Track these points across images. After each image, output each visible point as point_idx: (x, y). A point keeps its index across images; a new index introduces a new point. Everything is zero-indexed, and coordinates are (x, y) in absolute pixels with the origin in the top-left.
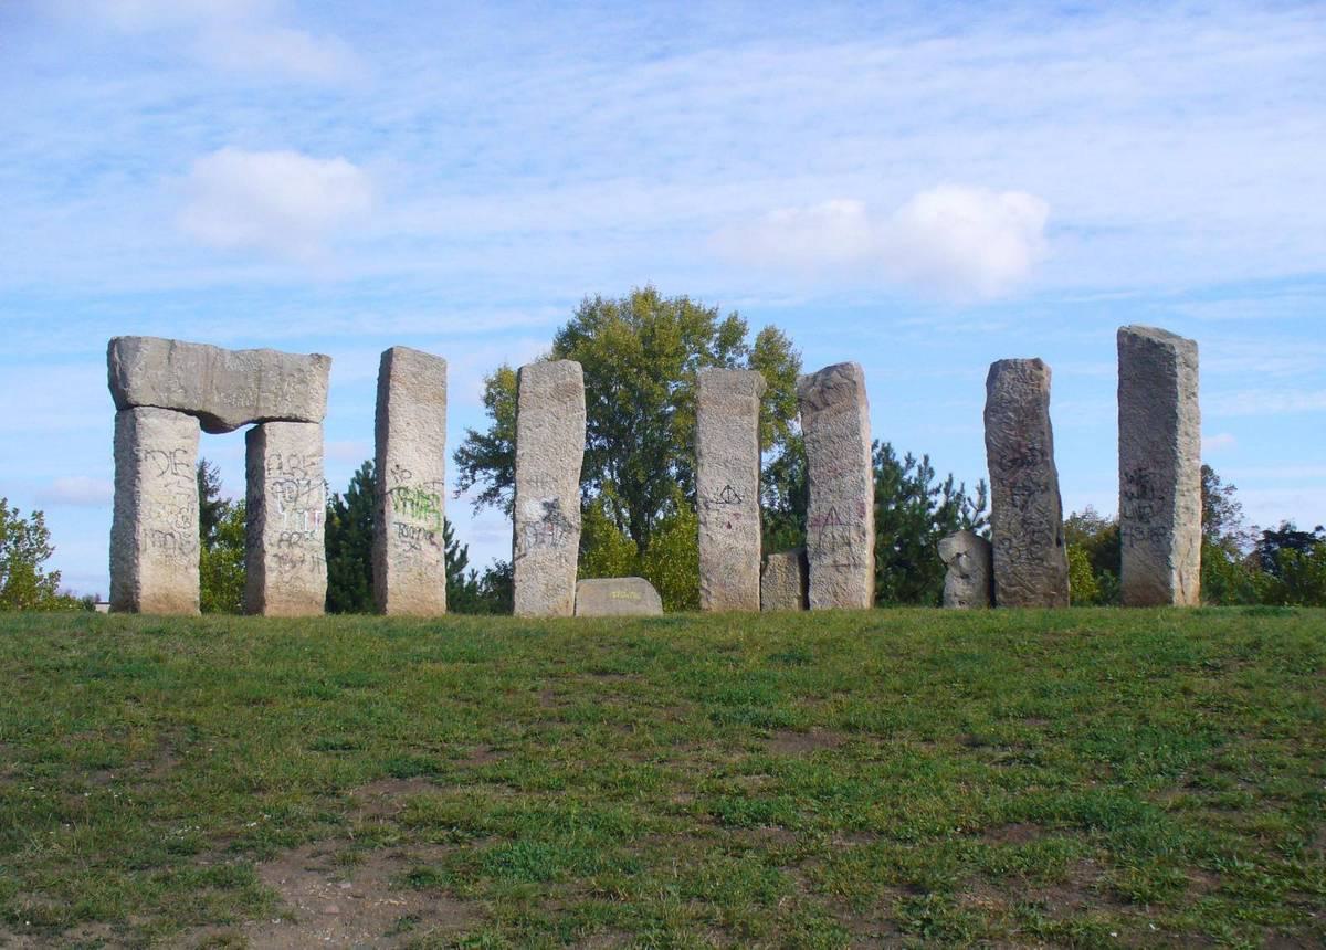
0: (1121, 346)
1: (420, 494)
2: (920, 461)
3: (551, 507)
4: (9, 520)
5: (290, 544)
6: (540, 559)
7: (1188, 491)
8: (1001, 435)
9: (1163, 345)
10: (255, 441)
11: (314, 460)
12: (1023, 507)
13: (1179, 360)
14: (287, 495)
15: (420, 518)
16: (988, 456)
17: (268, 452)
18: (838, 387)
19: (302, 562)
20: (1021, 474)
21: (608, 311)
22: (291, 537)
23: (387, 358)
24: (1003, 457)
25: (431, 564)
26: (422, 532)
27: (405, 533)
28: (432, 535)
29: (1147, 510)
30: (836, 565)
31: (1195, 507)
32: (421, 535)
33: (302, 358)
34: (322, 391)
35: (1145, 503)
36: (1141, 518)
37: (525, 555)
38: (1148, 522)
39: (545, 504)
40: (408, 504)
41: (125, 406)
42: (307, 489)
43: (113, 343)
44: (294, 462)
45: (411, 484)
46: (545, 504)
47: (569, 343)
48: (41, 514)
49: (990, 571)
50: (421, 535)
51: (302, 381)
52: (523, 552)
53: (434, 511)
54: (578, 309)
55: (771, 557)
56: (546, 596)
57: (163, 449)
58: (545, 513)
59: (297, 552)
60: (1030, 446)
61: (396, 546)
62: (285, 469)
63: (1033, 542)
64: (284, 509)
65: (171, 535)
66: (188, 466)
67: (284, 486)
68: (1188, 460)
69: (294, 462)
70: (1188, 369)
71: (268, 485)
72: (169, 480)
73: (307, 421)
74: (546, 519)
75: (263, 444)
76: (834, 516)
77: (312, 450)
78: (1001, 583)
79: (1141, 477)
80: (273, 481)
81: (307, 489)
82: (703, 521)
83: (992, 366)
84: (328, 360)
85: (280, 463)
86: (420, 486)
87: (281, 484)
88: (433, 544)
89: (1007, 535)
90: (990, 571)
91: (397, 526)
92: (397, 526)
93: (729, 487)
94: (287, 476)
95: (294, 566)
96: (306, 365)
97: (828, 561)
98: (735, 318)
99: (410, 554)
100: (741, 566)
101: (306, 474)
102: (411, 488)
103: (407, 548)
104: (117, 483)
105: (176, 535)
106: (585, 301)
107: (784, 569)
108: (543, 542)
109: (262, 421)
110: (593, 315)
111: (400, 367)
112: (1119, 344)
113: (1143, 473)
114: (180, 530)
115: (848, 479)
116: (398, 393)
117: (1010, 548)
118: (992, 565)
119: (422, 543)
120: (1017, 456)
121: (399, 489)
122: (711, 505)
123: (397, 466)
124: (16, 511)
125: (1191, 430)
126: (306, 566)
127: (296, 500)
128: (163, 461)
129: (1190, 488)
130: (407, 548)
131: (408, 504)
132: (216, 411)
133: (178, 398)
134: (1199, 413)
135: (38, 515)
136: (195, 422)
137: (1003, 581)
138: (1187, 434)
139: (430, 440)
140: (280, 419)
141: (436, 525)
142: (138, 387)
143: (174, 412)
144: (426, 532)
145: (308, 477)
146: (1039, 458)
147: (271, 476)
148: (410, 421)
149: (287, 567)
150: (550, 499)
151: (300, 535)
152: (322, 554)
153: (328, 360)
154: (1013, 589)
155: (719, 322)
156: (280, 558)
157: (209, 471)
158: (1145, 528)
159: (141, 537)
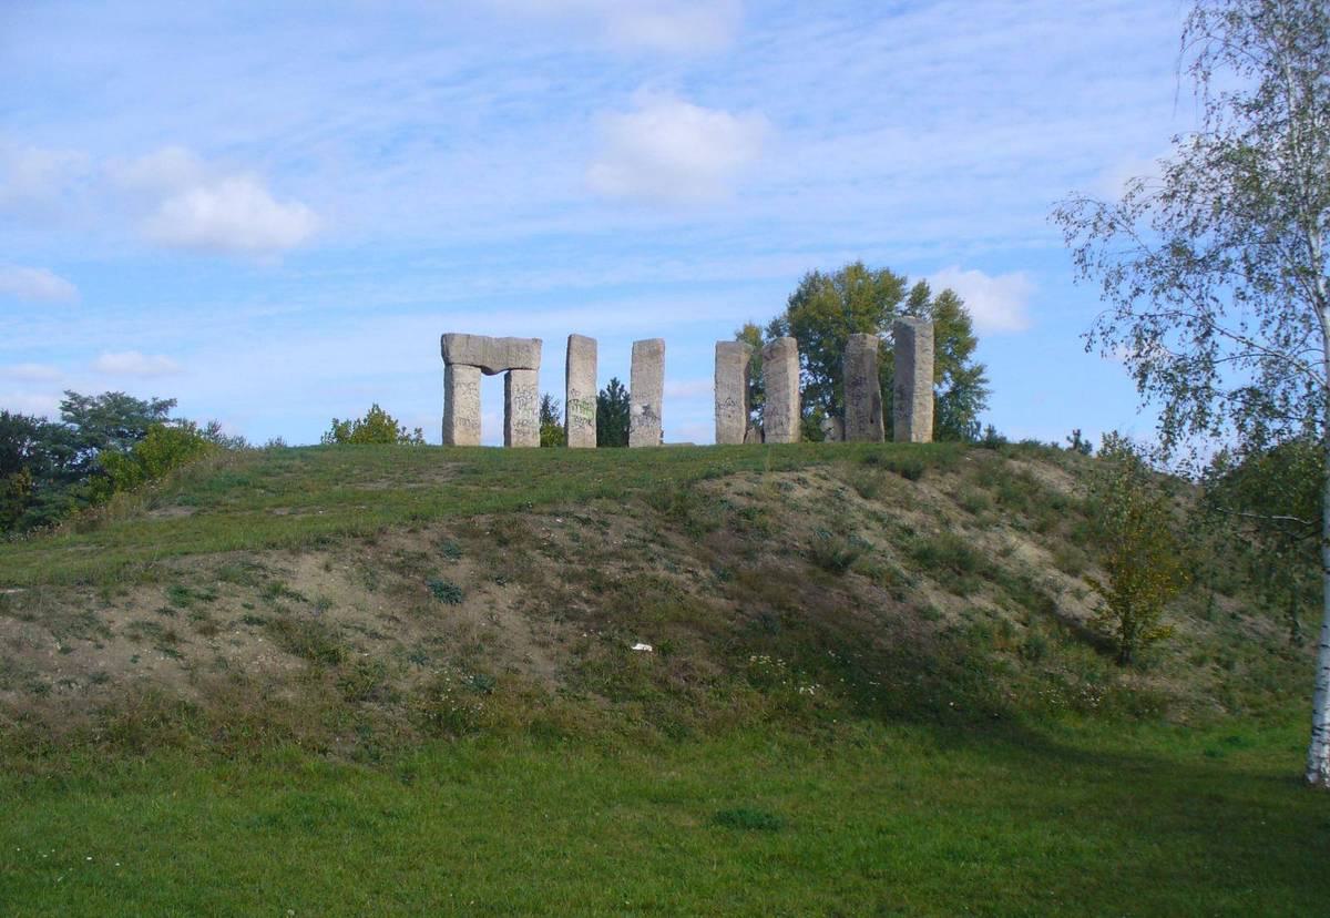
4: (399, 434)
5: (523, 425)
10: (508, 378)
13: (917, 334)
17: (512, 384)
18: (777, 349)
21: (825, 281)
23: (570, 338)
30: (776, 434)
33: (528, 340)
41: (448, 364)
43: (443, 336)
48: (420, 430)
51: (528, 351)
54: (803, 280)
59: (526, 429)
71: (512, 399)
74: (644, 414)
75: (510, 380)
96: (530, 344)
97: (773, 432)
98: (924, 283)
104: (445, 398)
106: (808, 274)
109: (510, 369)
111: (574, 342)
115: (783, 393)
116: (573, 353)
124: (404, 429)
126: (530, 435)
132: (488, 366)
133: (471, 360)
135: (418, 431)
136: (479, 370)
142: (453, 353)
147: (514, 394)
155: (911, 285)
156: (518, 431)
157: (551, 403)
159: (454, 421)
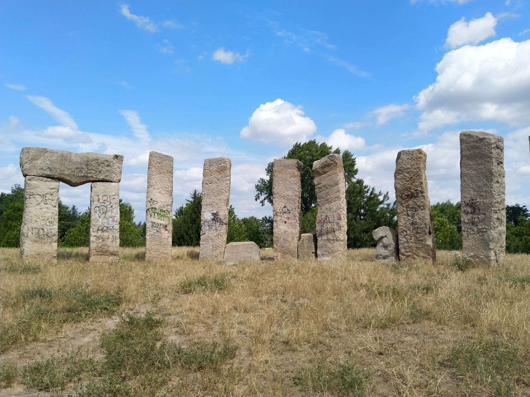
0: (461, 141)
1: (161, 210)
2: (371, 190)
3: (215, 215)
6: (210, 235)
7: (499, 210)
8: (402, 184)
9: (485, 139)
11: (114, 197)
12: (413, 217)
14: (101, 211)
15: (161, 220)
16: (396, 193)
19: (108, 238)
20: (411, 202)
22: (103, 228)
24: (403, 194)
25: (165, 238)
26: (162, 225)
27: (154, 226)
28: (166, 226)
29: (476, 220)
30: (328, 240)
31: (502, 218)
32: (161, 227)
34: (118, 170)
35: (475, 216)
36: (473, 223)
37: (204, 234)
38: (477, 225)
39: (213, 214)
40: (156, 214)
42: (111, 209)
44: (105, 198)
45: (157, 206)
46: (213, 214)
47: (292, 154)
49: (397, 245)
50: (161, 227)
52: (204, 233)
53: (167, 217)
55: (302, 235)
56: (213, 251)
57: (40, 193)
58: (212, 217)
59: (106, 234)
60: (416, 189)
61: (150, 231)
62: (101, 201)
63: (417, 233)
64: (100, 217)
65: (42, 229)
66: (53, 200)
67: (100, 208)
68: (499, 195)
69: (105, 198)
70: (498, 150)
72: (42, 207)
73: (111, 182)
74: (213, 220)
76: (328, 219)
77: (113, 193)
78: (402, 251)
79: (473, 203)
80: (95, 206)
81: (111, 209)
82: (275, 220)
83: (398, 153)
84: (122, 157)
85: (99, 199)
86: (161, 207)
87: (99, 207)
88: (167, 230)
89: (405, 229)
90: (397, 245)
91: (151, 223)
92: (151, 223)
93: (285, 207)
94: (102, 204)
95: (104, 240)
97: (325, 238)
99: (157, 234)
100: (290, 239)
101: (110, 203)
102: (157, 208)
103: (155, 232)
105: (45, 229)
107: (307, 241)
108: (212, 229)
110: (297, 147)
112: (460, 139)
113: (474, 201)
114: (48, 227)
117: (406, 235)
118: (399, 247)
119: (162, 230)
120: (409, 193)
121: (152, 208)
122: (279, 214)
123: (151, 199)
125: (500, 180)
127: (106, 213)
128: (39, 199)
129: (500, 209)
130: (155, 232)
131: (156, 214)
134: (504, 171)
137: (403, 250)
138: (498, 182)
139: (166, 189)
140: (99, 181)
141: (168, 222)
143: (46, 178)
144: (163, 225)
145: (111, 204)
146: (420, 195)
148: (157, 181)
149: (100, 241)
150: (215, 212)
151: (107, 228)
152: (118, 235)
153: (122, 157)
154: (408, 254)
158: (475, 229)
